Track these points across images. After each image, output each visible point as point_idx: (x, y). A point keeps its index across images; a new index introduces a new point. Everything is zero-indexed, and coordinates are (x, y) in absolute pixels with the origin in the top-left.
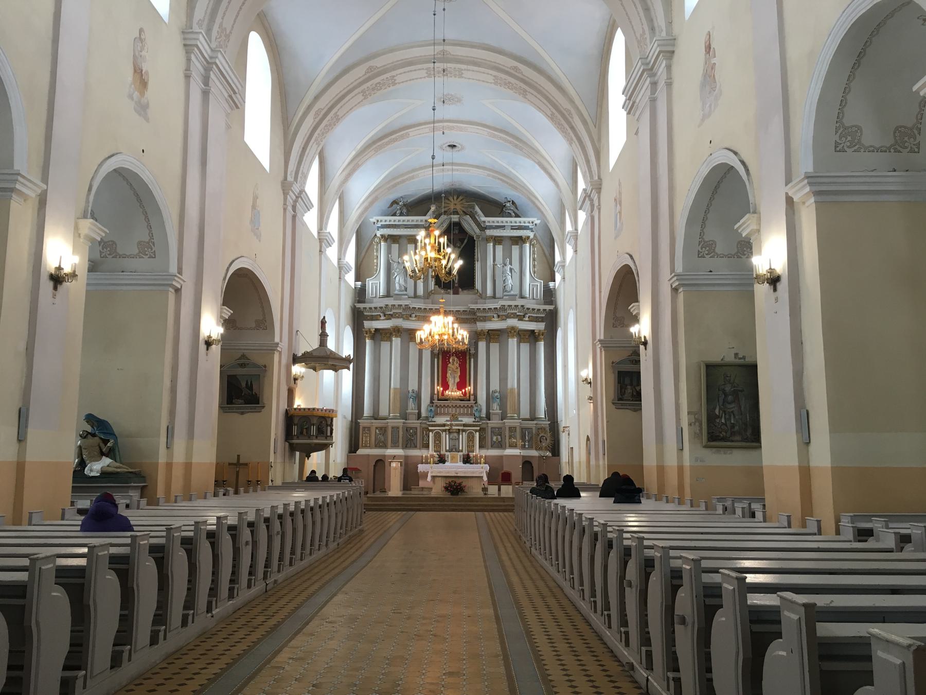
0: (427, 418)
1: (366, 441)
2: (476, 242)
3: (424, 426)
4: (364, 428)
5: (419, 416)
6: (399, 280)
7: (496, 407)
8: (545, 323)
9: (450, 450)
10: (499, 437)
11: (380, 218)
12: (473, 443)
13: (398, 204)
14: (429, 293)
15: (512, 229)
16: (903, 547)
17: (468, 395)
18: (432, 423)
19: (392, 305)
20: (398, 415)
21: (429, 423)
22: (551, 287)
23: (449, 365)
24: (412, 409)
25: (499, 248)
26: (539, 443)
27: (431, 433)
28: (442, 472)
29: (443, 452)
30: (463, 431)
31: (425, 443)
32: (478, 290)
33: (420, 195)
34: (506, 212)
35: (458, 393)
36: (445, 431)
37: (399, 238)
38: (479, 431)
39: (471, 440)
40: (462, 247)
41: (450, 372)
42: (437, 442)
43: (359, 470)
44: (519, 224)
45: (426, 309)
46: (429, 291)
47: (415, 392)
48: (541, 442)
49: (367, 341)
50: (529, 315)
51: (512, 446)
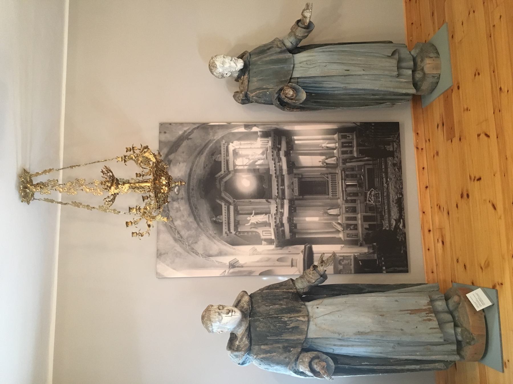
16: (272, 104)
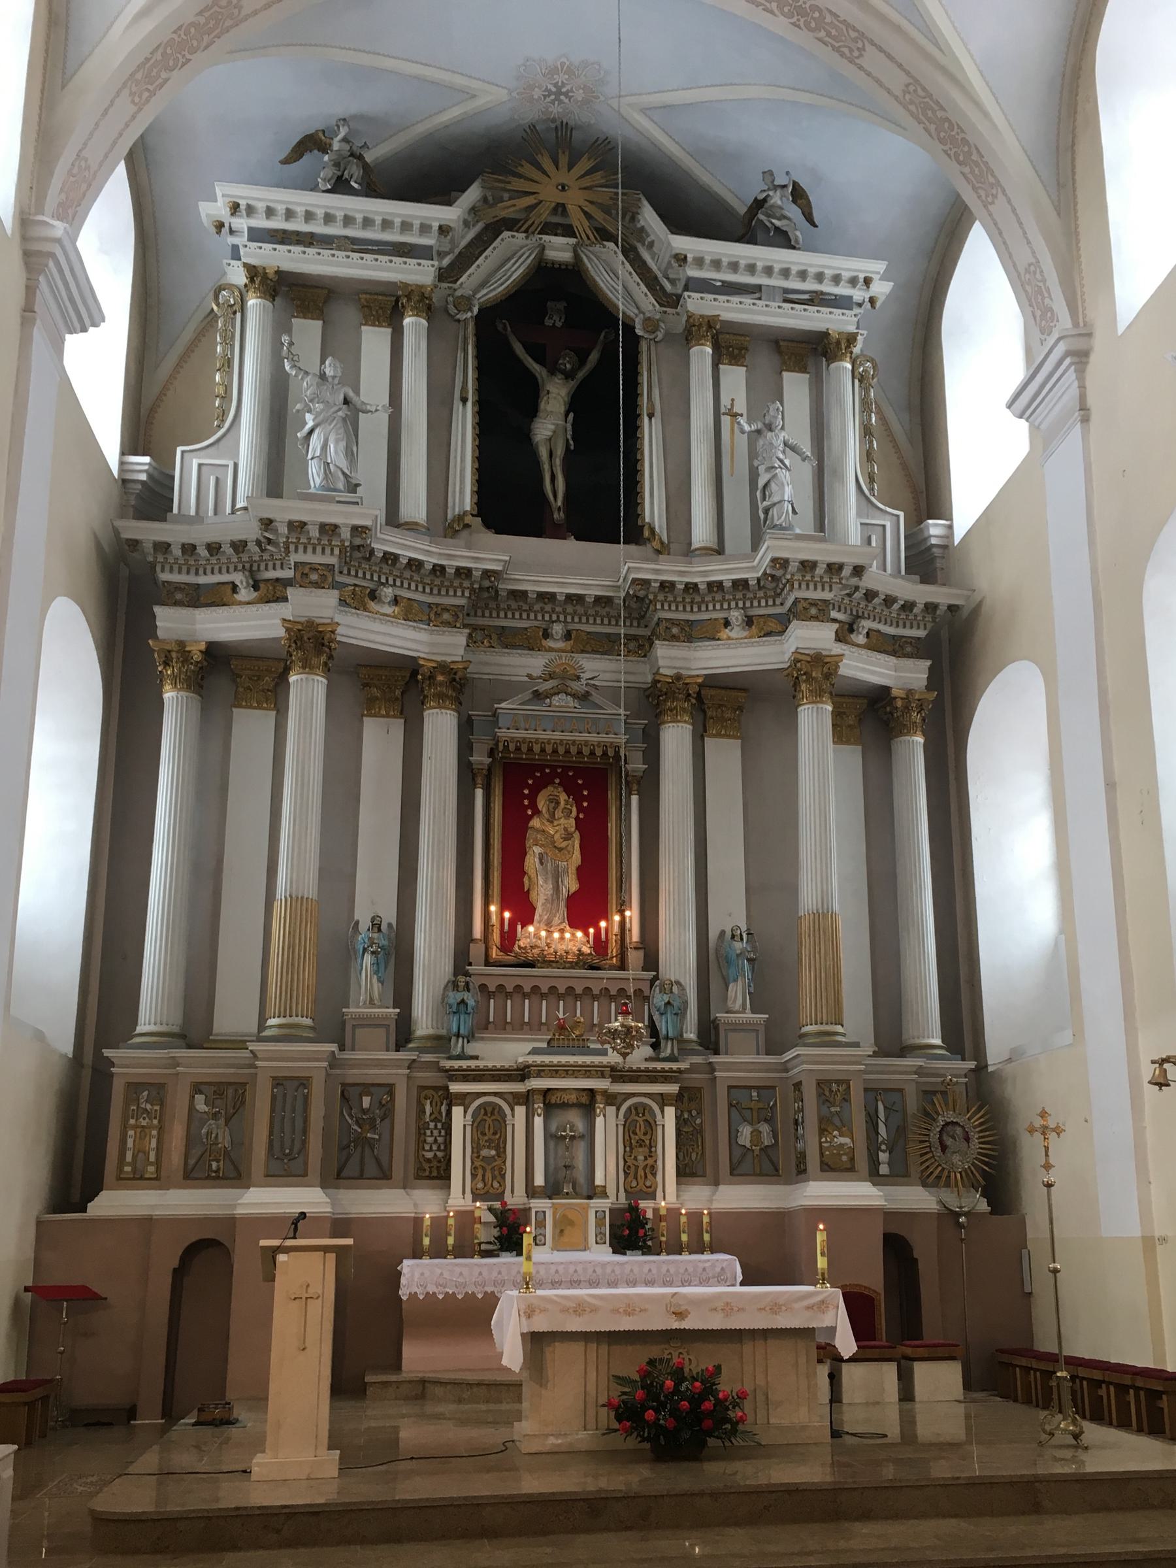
0: (440, 1043)
1: (140, 1151)
2: (644, 346)
3: (428, 1077)
4: (134, 1088)
5: (403, 1034)
6: (325, 447)
7: (739, 1001)
8: (929, 663)
9: (552, 1190)
10: (765, 1128)
11: (245, 193)
12: (651, 1154)
13: (324, 148)
14: (451, 526)
15: (786, 301)
17: (613, 949)
18: (464, 1064)
19: (291, 524)
20: (308, 1022)
21: (448, 1064)
22: (933, 541)
23: (535, 823)
24: (372, 1003)
25: (735, 378)
26: (938, 1153)
27: (457, 1111)
28: (594, 1310)
29: (516, 1198)
30: (612, 1099)
31: (429, 1155)
32: (652, 531)
33: (421, 129)
34: (768, 229)
35: (575, 941)
36: (525, 1099)
37: (327, 299)
38: (677, 1100)
39: (641, 1143)
40: (581, 375)
41: (537, 850)
42: (485, 1152)
43: (96, 1297)
44: (816, 287)
45: (443, 568)
46: (450, 516)
47: (384, 927)
48: (944, 1148)
49: (170, 695)
50: (875, 625)
51: (836, 1167)
